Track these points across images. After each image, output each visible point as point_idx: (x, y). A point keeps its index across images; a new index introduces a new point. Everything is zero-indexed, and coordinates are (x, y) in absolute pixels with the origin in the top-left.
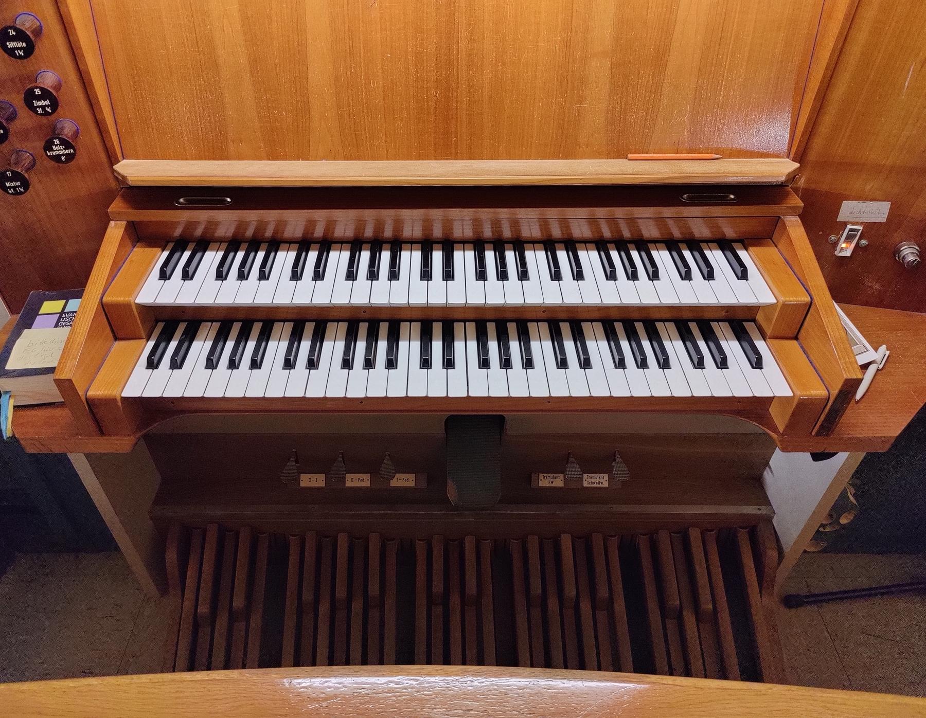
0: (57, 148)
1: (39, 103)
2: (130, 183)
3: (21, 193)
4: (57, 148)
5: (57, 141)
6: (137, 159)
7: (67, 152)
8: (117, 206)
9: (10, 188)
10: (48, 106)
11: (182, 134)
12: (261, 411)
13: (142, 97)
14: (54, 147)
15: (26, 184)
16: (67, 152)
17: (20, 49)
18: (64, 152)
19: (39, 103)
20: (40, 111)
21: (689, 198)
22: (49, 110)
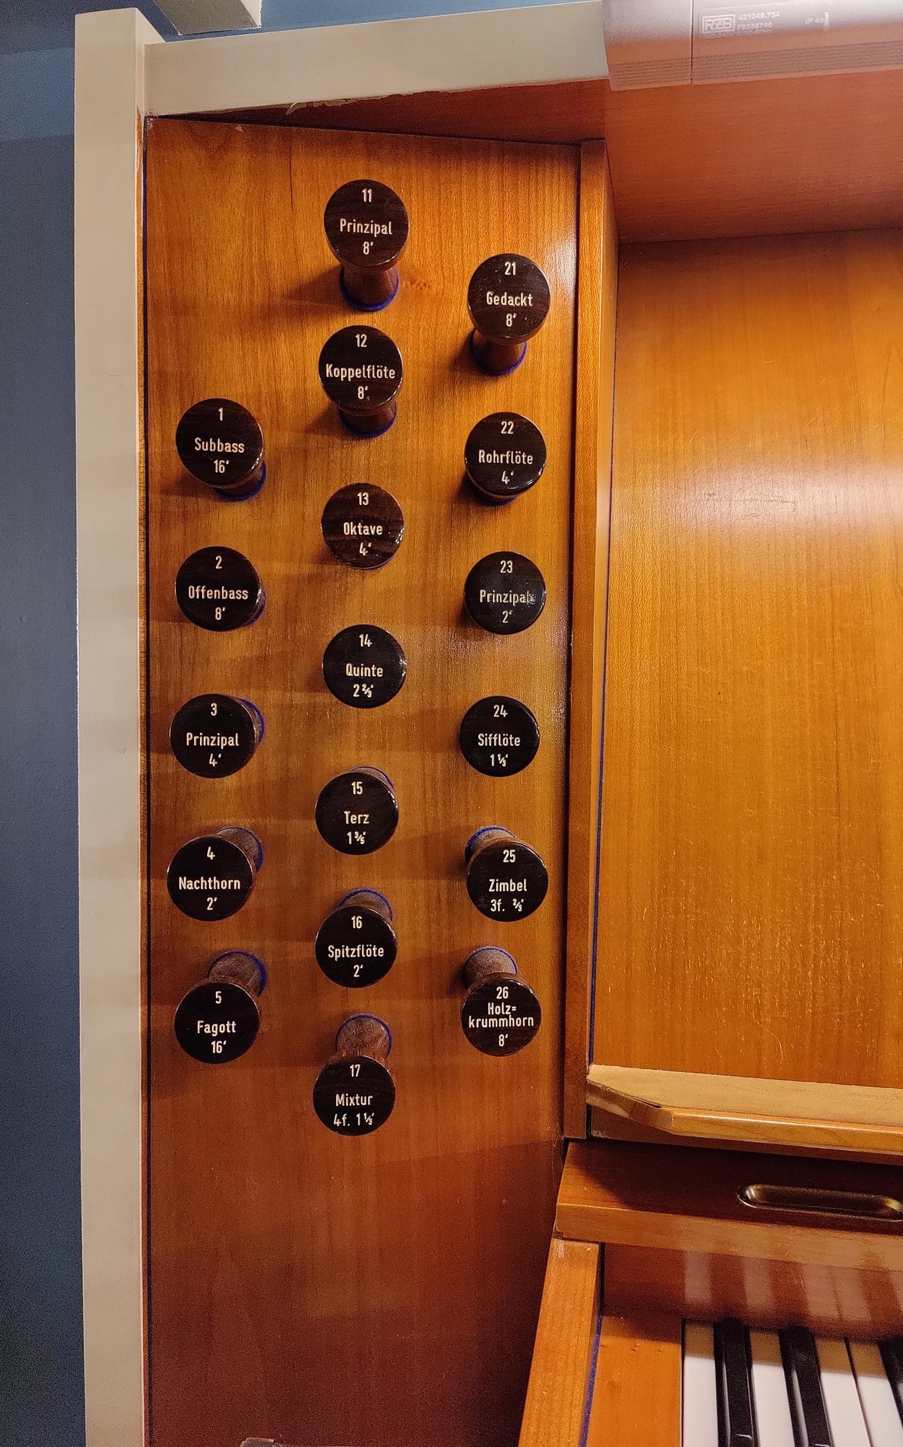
0: (498, 1010)
1: (503, 886)
2: (674, 1128)
3: (365, 1129)
4: (498, 1010)
5: (503, 992)
6: (627, 1065)
7: (519, 1022)
8: (575, 1193)
9: (341, 1110)
10: (518, 895)
11: (759, 1006)
12: (149, 906)
13: (677, 912)
14: (491, 1008)
15: (382, 1108)
16: (519, 1022)
17: (502, 750)
18: (511, 1022)
19: (503, 886)
20: (496, 905)
21: (768, 1198)
22: (518, 906)
